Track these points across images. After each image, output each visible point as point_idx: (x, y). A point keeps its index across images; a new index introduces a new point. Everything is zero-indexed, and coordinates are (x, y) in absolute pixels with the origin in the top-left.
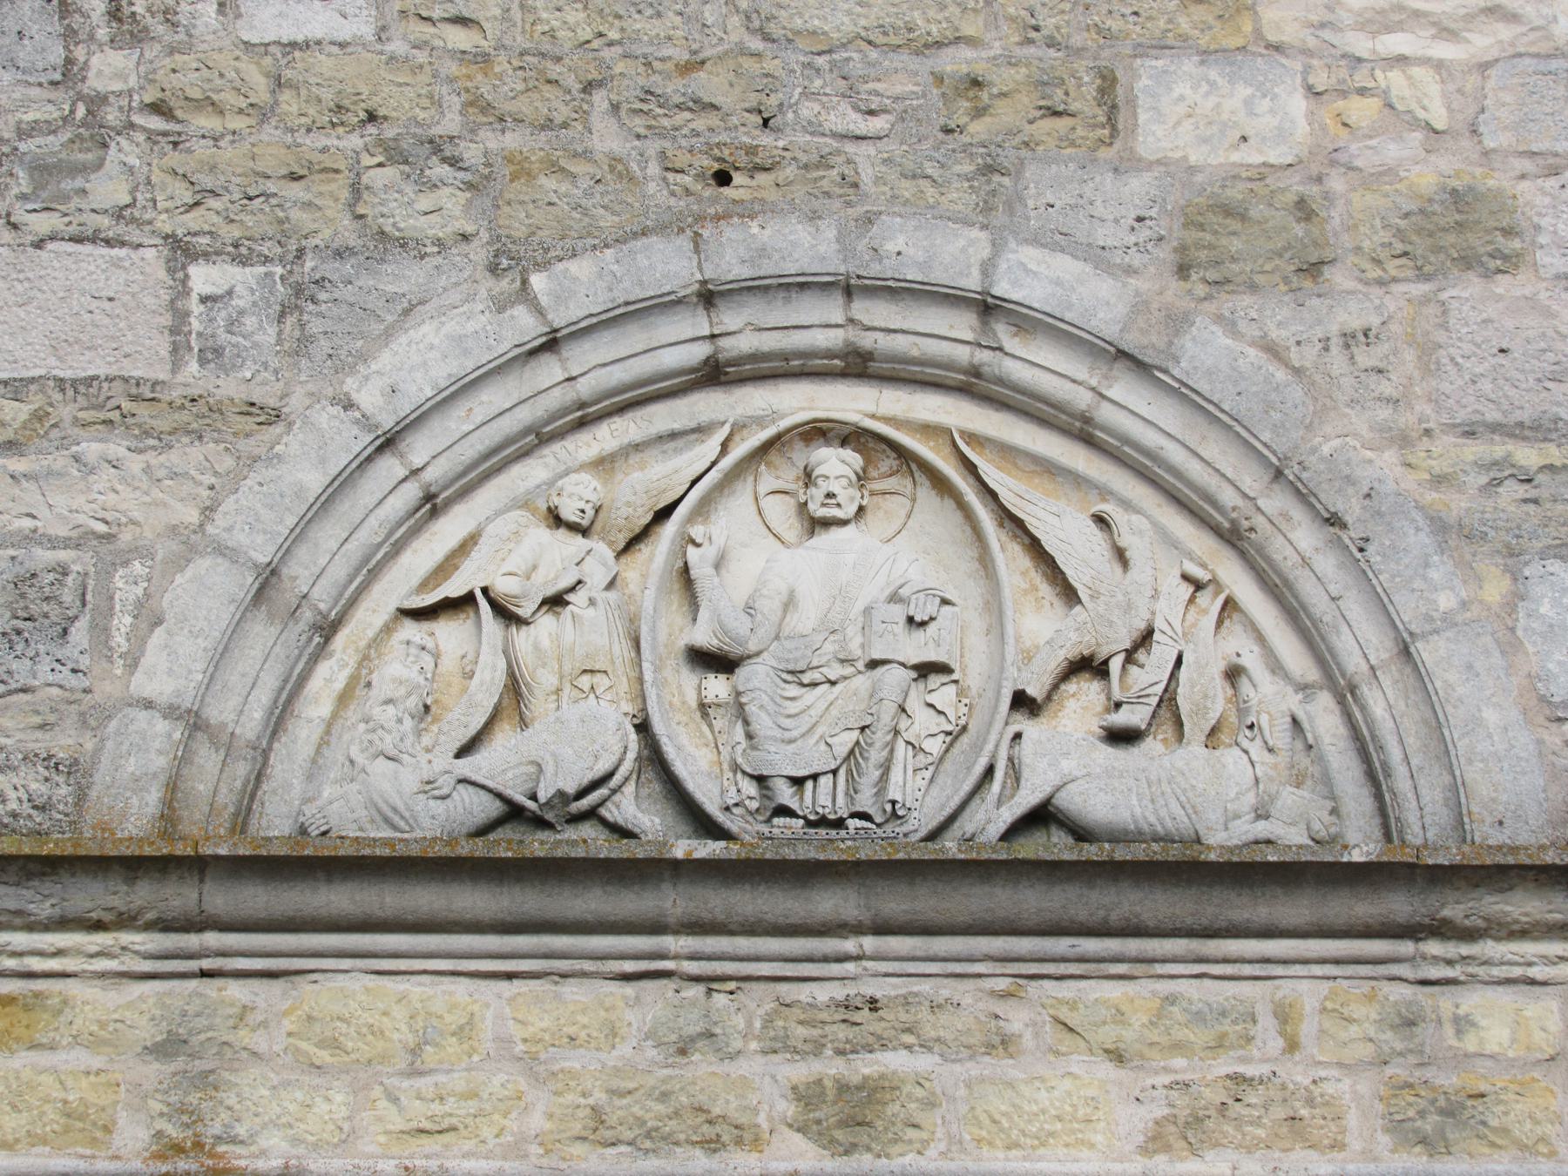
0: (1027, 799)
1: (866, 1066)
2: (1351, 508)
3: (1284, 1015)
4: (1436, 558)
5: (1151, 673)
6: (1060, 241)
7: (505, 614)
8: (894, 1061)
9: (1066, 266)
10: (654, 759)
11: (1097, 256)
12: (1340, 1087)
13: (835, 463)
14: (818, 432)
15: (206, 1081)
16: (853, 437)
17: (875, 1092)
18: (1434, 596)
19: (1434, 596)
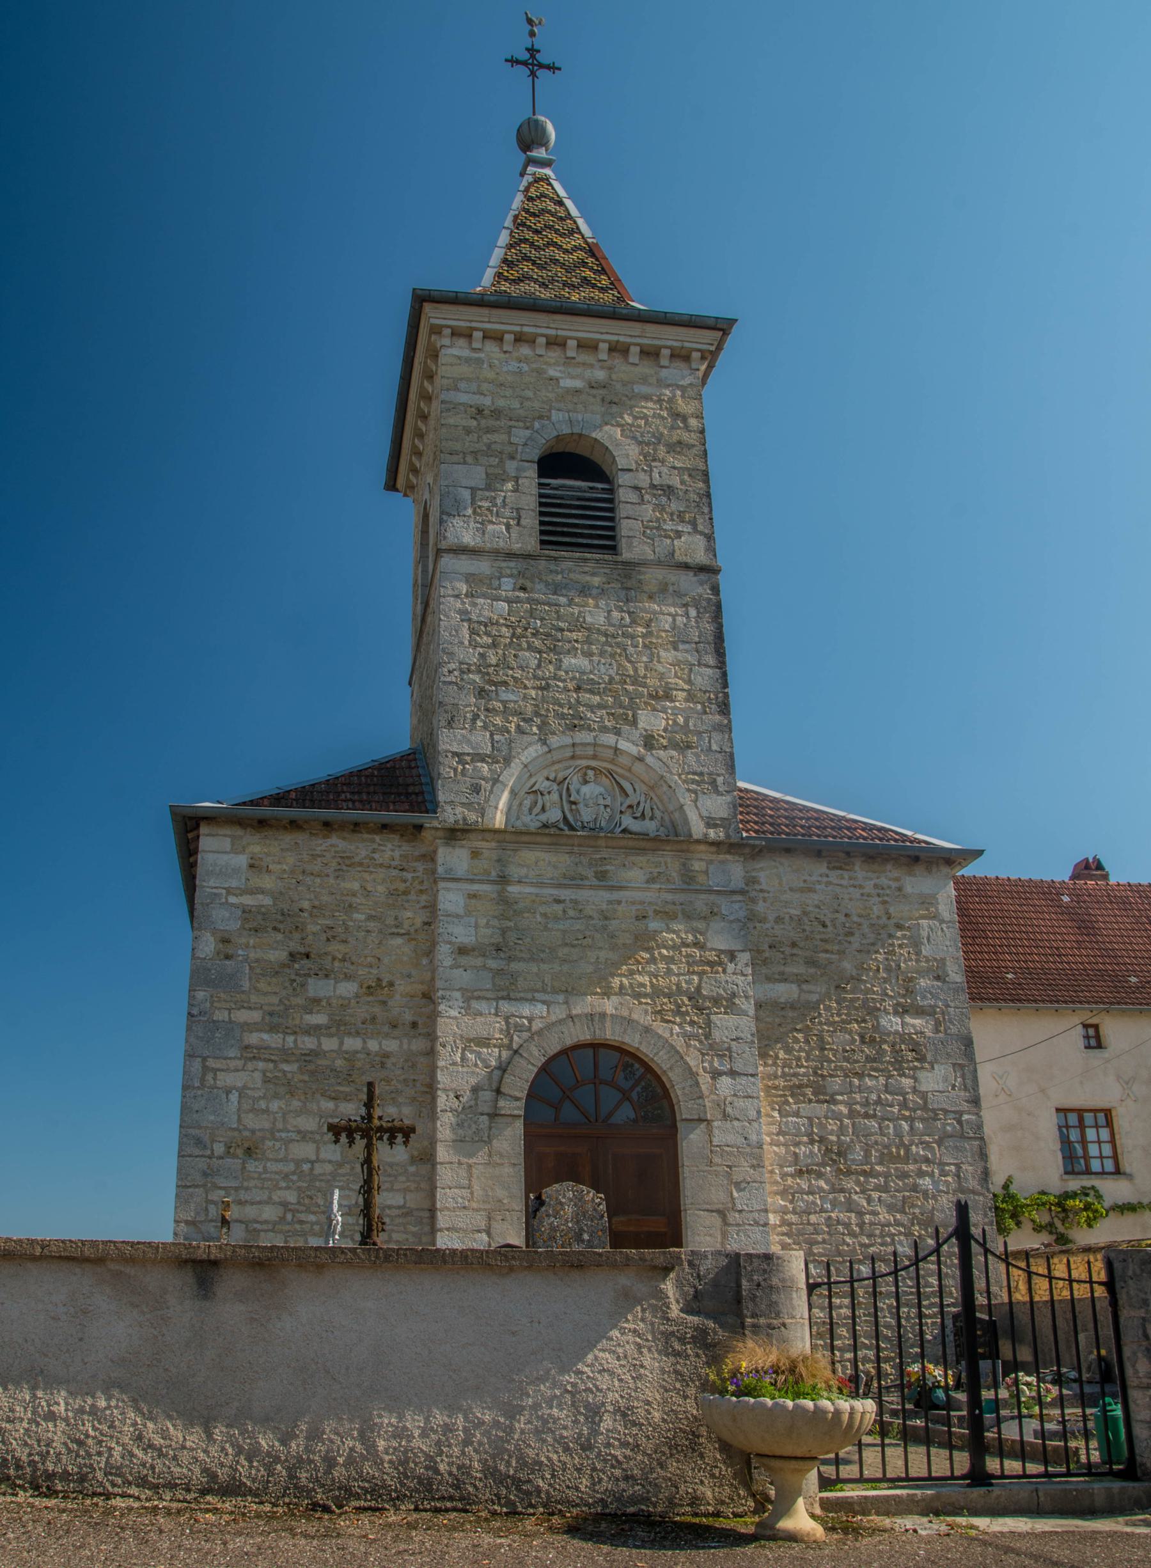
0: (623, 827)
1: (604, 868)
2: (673, 785)
3: (666, 863)
4: (341, 1460)
5: (641, 808)
6: (628, 740)
7: (542, 794)
8: (608, 867)
9: (630, 745)
10: (565, 818)
11: (633, 743)
12: (674, 874)
13: (591, 773)
14: (588, 767)
15: (504, 866)
16: (593, 769)
17: (606, 872)
18: (790, 1395)
19: (790, 1395)
